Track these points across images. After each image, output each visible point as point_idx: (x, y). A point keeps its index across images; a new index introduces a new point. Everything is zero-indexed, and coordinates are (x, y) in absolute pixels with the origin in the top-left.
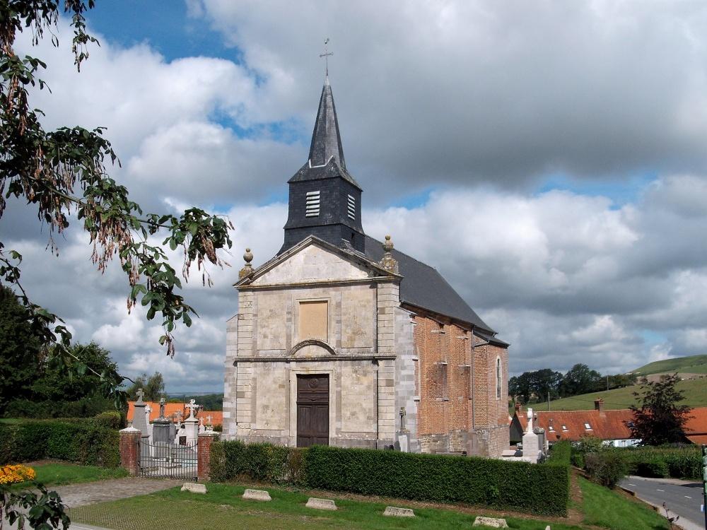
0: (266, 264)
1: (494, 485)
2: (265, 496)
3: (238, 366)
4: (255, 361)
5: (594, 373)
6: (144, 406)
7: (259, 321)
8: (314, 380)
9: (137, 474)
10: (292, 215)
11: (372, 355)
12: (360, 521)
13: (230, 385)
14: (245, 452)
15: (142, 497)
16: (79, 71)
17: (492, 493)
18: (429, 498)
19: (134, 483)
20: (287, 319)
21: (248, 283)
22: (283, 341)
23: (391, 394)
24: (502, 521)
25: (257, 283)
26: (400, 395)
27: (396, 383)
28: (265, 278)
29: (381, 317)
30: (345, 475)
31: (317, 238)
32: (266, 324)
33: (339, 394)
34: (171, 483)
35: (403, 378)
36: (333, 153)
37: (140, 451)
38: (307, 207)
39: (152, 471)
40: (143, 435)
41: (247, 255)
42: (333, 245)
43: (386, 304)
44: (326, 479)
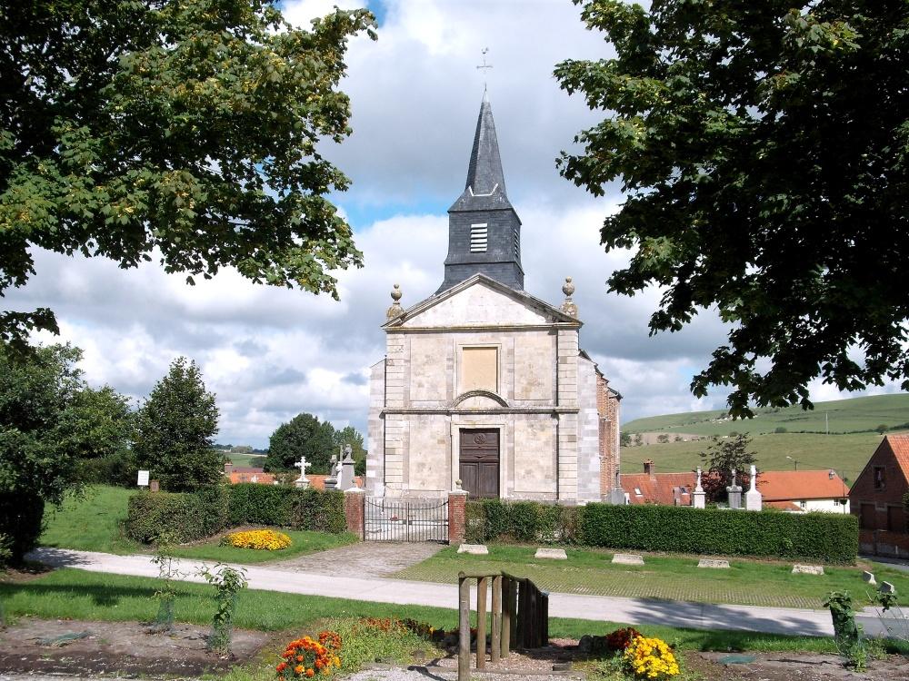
8: (480, 434)
13: (375, 440)
22: (443, 391)
23: (574, 450)
27: (579, 439)
30: (628, 532)
32: (422, 372)
41: (396, 292)
43: (569, 353)
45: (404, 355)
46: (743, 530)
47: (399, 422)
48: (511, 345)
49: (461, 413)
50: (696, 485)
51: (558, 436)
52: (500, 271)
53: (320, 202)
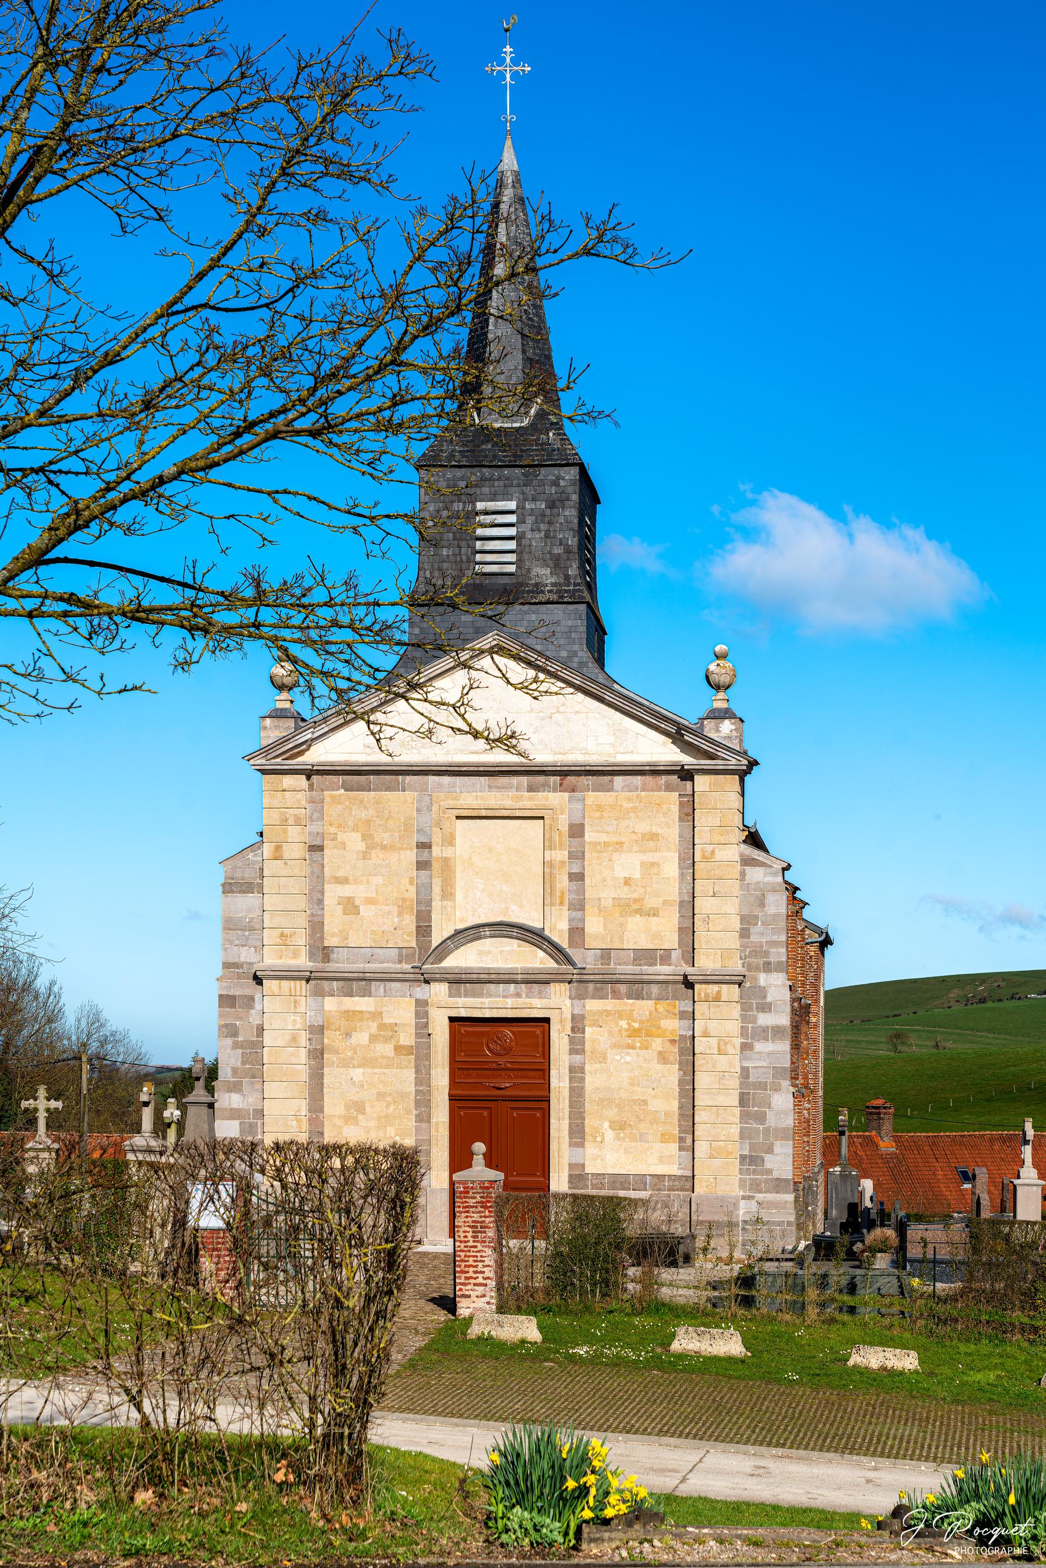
16: (155, 693)
53: (224, 1030)
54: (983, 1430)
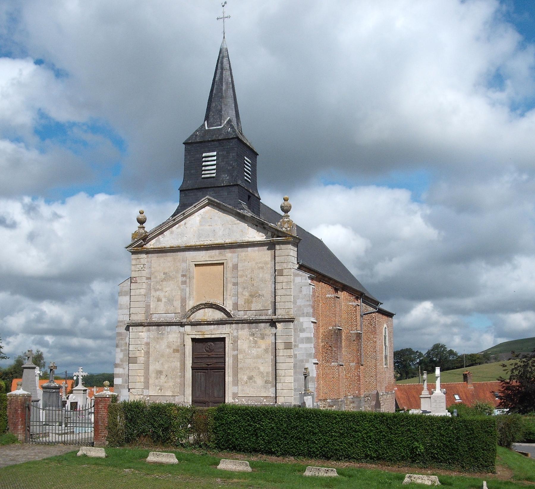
0: (161, 226)
1: (418, 442)
2: (172, 459)
3: (131, 330)
4: (148, 326)
5: (451, 352)
6: (34, 368)
7: (152, 284)
8: (209, 344)
9: (26, 441)
10: (187, 176)
11: (270, 317)
12: (281, 482)
13: (122, 351)
14: (146, 413)
15: (35, 463)
17: (417, 450)
18: (348, 458)
19: (23, 449)
20: (182, 282)
21: (141, 246)
22: (177, 304)
23: (290, 357)
24: (435, 478)
25: (151, 245)
26: (299, 357)
27: (295, 346)
28: (158, 241)
29: (279, 279)
30: (256, 435)
31: (213, 199)
32: (160, 288)
33: (236, 358)
34: (65, 449)
35: (302, 341)
36: (229, 115)
37: (30, 415)
38: (203, 168)
39: (43, 437)
40: (33, 399)
41: (141, 217)
42: (230, 207)
43: (285, 265)
44: (237, 439)
45: (145, 273)
46: (372, 434)
47: (140, 333)
48: (235, 260)
49: (193, 324)
50: (422, 389)
51: (276, 343)
52: (226, 194)
54: (79, 433)
